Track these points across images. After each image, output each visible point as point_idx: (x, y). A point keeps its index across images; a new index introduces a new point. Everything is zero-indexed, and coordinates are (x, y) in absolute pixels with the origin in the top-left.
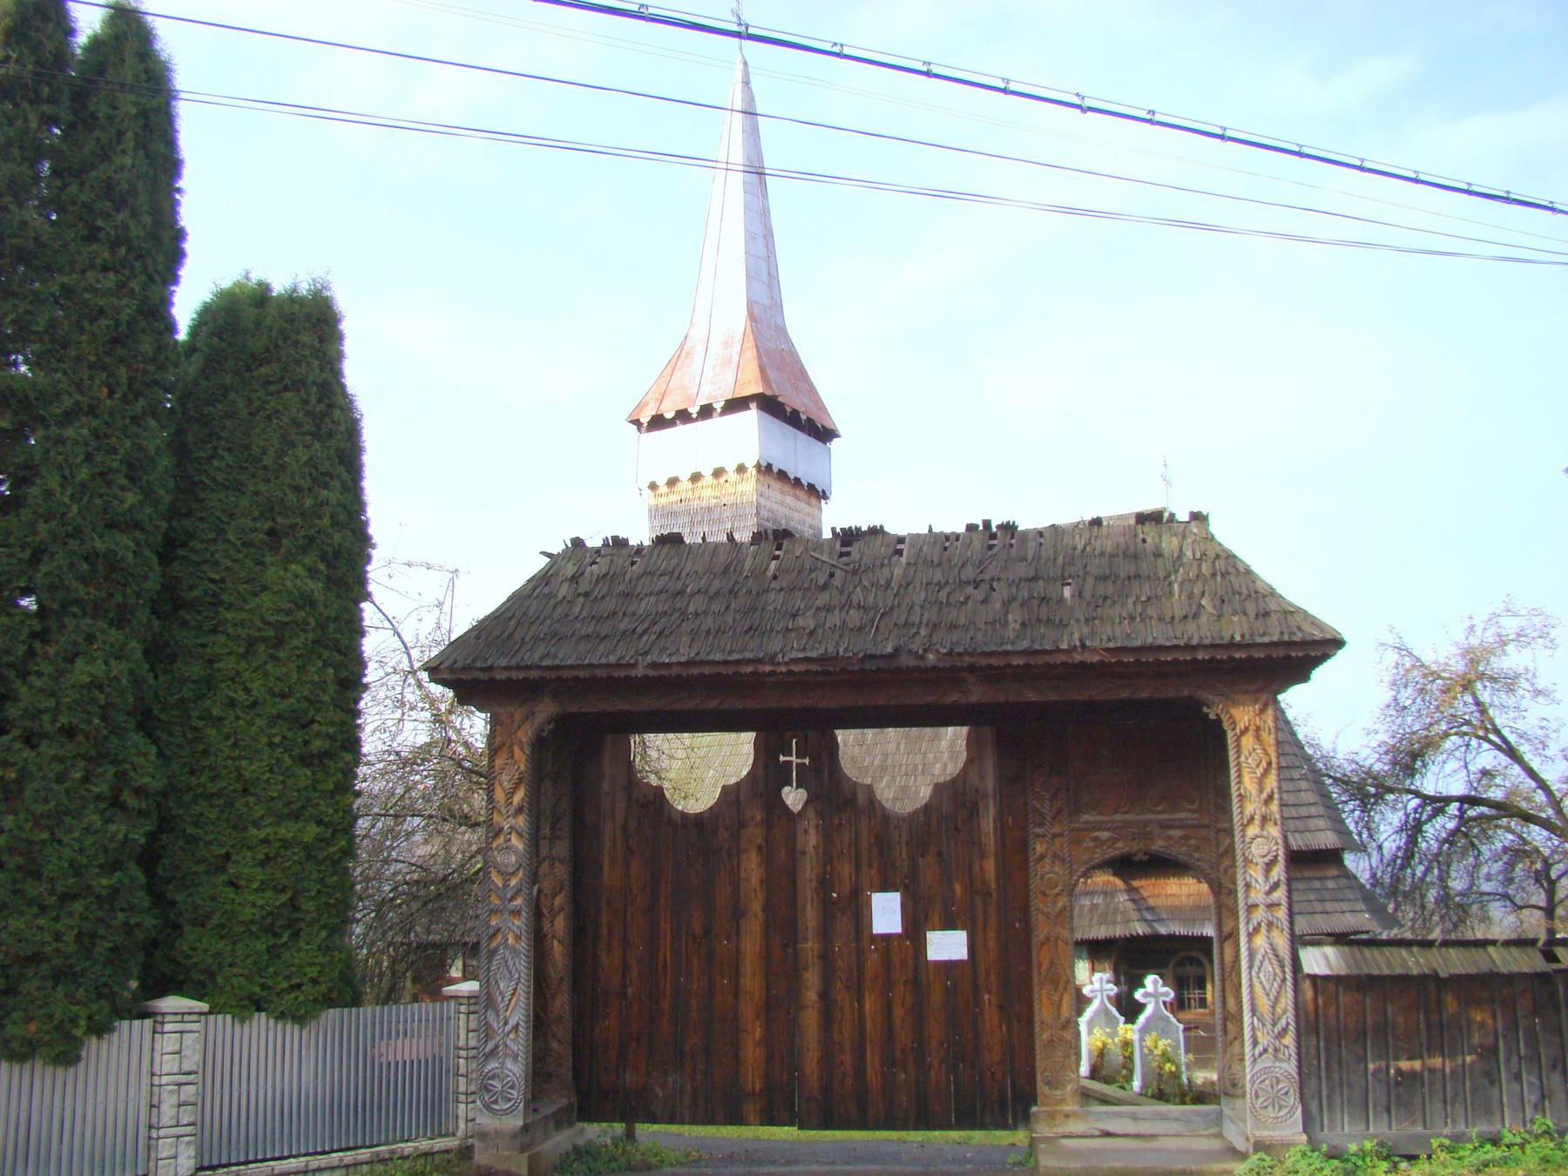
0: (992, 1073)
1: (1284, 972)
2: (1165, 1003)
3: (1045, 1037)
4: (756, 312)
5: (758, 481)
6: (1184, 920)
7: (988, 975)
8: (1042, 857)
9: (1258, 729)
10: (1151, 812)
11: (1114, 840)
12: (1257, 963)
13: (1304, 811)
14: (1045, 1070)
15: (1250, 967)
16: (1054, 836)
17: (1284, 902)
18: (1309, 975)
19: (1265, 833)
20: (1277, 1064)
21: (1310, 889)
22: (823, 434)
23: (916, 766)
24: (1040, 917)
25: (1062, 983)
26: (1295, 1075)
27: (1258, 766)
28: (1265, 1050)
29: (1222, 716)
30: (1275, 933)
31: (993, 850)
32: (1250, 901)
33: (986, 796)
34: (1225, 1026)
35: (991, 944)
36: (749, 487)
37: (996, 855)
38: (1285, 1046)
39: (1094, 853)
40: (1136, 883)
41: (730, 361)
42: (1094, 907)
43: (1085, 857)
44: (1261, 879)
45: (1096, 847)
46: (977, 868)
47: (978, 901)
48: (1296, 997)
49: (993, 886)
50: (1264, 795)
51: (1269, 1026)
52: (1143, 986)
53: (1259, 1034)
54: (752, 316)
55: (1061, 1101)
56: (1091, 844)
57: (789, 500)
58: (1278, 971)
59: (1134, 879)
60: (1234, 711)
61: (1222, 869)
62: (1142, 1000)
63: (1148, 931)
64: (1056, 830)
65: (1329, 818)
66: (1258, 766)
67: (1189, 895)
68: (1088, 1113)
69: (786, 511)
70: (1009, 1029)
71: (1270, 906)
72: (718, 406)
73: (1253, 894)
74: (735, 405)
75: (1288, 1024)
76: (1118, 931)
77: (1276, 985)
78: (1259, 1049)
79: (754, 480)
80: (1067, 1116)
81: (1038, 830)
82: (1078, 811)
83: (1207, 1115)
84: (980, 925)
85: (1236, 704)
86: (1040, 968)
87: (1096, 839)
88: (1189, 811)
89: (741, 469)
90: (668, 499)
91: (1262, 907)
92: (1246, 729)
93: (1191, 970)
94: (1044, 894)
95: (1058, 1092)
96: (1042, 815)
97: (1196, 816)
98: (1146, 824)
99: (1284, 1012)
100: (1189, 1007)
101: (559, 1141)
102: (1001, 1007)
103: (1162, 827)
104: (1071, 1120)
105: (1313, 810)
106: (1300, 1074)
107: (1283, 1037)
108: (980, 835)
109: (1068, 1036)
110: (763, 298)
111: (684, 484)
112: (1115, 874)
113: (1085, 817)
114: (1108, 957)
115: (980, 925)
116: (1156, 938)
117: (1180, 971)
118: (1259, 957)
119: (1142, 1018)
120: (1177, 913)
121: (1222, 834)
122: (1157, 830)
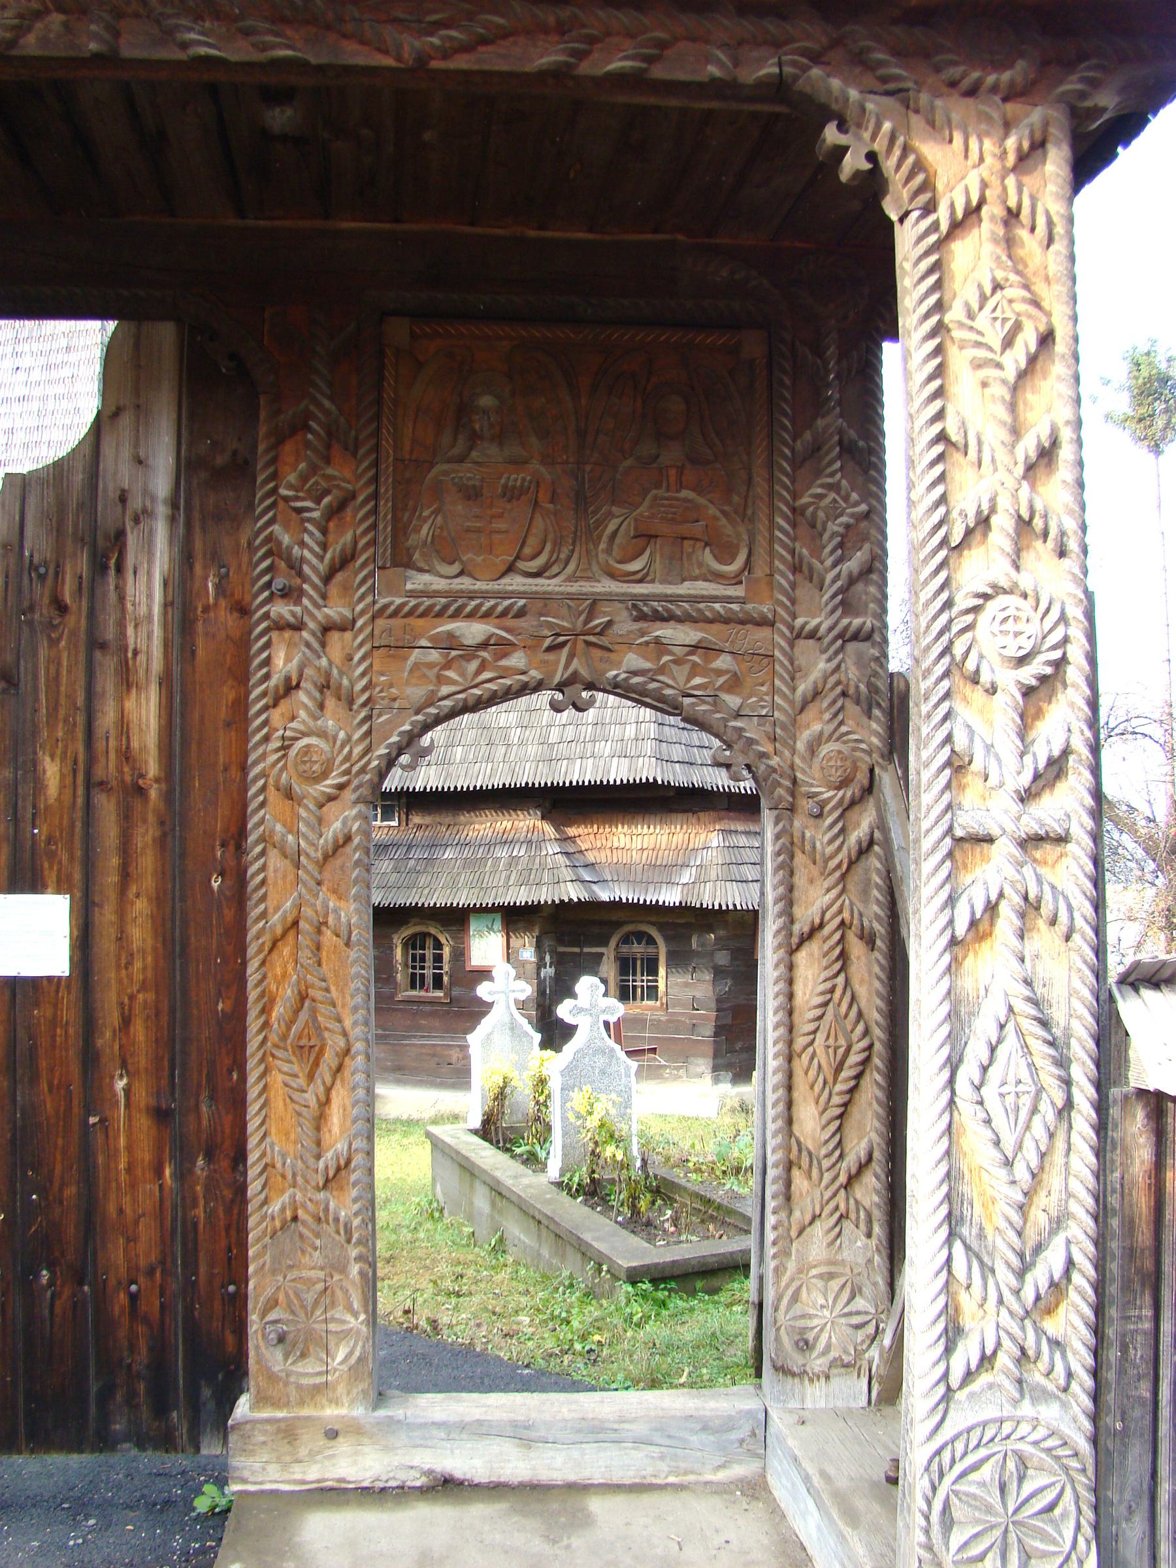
0: (134, 1298)
1: (1067, 1083)
2: (607, 1024)
3: (275, 1207)
6: (632, 883)
7: (126, 1021)
8: (290, 687)
9: (1012, 215)
10: (613, 575)
11: (503, 647)
12: (976, 1052)
14: (272, 1304)
15: (953, 1064)
16: (327, 629)
17: (1080, 827)
18: (1142, 1093)
19: (1025, 581)
20: (1026, 1408)
24: (275, 860)
25: (329, 1059)
26: (1085, 1447)
27: (1008, 343)
28: (987, 1360)
29: (889, 164)
30: (1044, 939)
31: (157, 665)
32: (966, 822)
33: (143, 516)
34: (788, 1183)
35: (140, 935)
37: (166, 680)
38: (1055, 1344)
39: (441, 680)
40: (572, 831)
42: (513, 860)
43: (416, 692)
44: (1008, 744)
45: (447, 665)
46: (107, 718)
47: (107, 808)
48: (1100, 1174)
49: (152, 768)
50: (1028, 446)
51: (1005, 1277)
52: (573, 996)
53: (967, 1303)
55: (318, 1391)
56: (435, 656)
58: (1049, 1076)
59: (570, 826)
60: (930, 151)
61: (800, 746)
62: (569, 1019)
63: (584, 896)
64: (335, 611)
66: (1008, 343)
67: (642, 849)
68: (392, 1424)
70: (183, 1175)
71: (1032, 842)
73: (972, 794)
75: (1070, 1264)
76: (545, 895)
77: (1038, 1129)
78: (967, 1353)
80: (333, 1434)
81: (282, 610)
82: (402, 560)
83: (728, 1424)
84: (110, 879)
85: (938, 128)
86: (265, 1010)
87: (450, 643)
88: (717, 577)
91: (1004, 849)
92: (973, 212)
93: (637, 949)
94: (289, 794)
95: (309, 1367)
96: (295, 567)
97: (738, 591)
98: (595, 604)
99: (1058, 1223)
100: (634, 998)
102: (161, 1115)
103: (642, 617)
104: (343, 1446)
106: (1095, 1441)
107: (1049, 1311)
108: (121, 625)
109: (344, 1206)
113: (418, 581)
114: (528, 928)
115: (110, 879)
116: (594, 906)
117: (625, 949)
118: (983, 1029)
119: (570, 1048)
120: (623, 872)
121: (802, 644)
122: (625, 626)
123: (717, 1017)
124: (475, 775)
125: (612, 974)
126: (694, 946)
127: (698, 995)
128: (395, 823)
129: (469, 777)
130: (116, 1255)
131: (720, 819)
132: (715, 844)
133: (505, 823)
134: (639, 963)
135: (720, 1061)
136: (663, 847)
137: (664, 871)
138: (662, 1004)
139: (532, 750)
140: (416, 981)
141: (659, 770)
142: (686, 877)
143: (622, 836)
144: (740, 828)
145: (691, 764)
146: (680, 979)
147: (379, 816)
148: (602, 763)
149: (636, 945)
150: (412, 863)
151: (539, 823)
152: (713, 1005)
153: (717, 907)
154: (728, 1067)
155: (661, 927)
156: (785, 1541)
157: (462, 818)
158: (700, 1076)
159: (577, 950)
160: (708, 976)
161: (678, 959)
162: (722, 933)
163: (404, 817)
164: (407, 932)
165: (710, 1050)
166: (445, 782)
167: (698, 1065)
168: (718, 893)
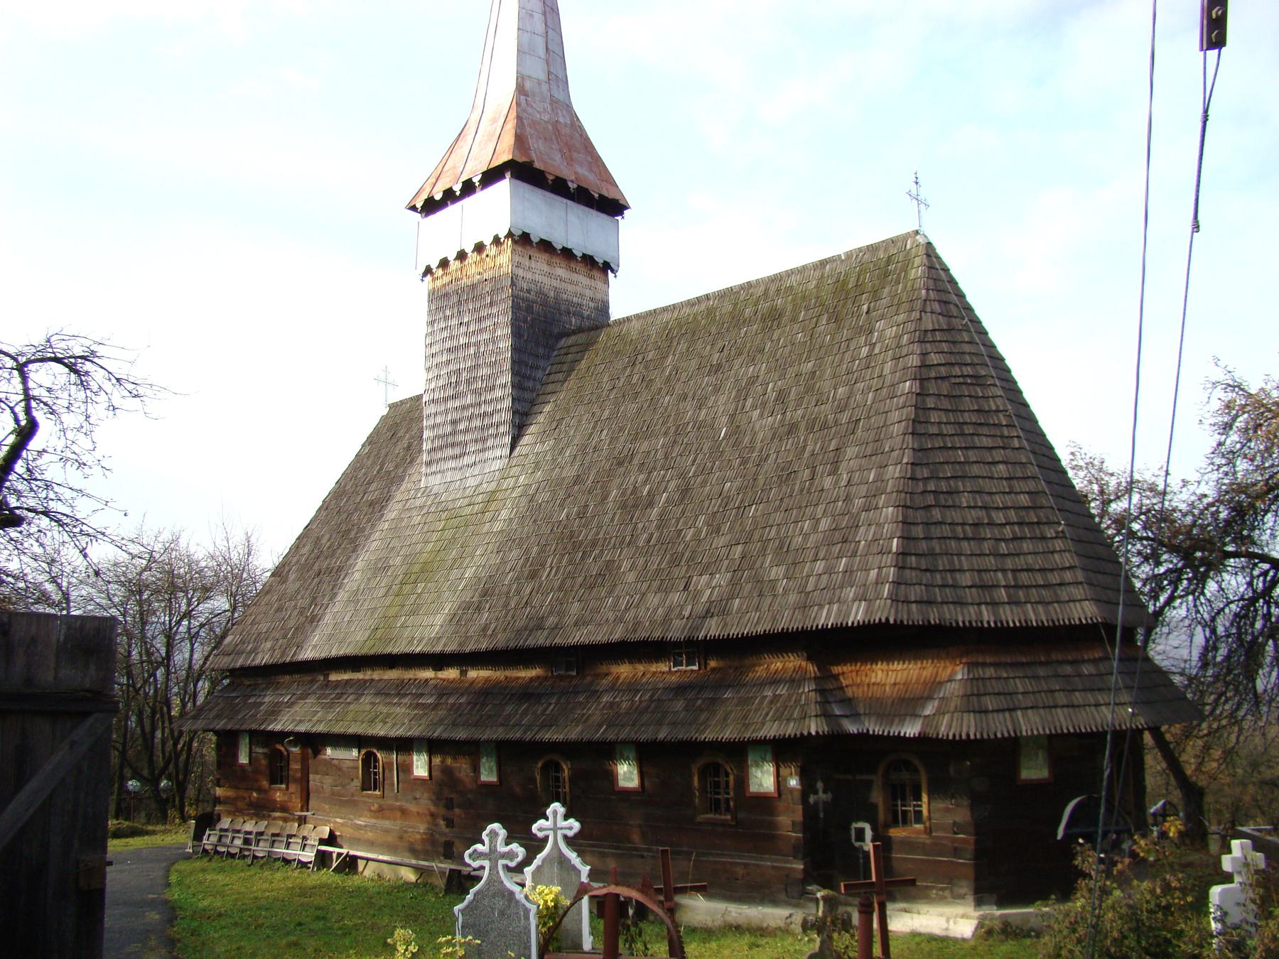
4: (528, 85)
5: (513, 251)
13: (1054, 578)
21: (1057, 676)
22: (613, 207)
23: (624, 537)
36: (504, 259)
41: (494, 134)
42: (776, 698)
54: (521, 90)
57: (561, 272)
59: (838, 664)
65: (1090, 584)
69: (556, 283)
72: (476, 180)
74: (491, 177)
79: (509, 251)
89: (497, 241)
90: (442, 279)
93: (905, 776)
101: (1276, 904)
105: (1068, 576)
110: (537, 70)
111: (454, 265)
112: (809, 659)
123: (976, 842)
124: (745, 622)
128: (695, 668)
129: (740, 625)
130: (247, 740)
132: (959, 677)
133: (778, 664)
136: (913, 682)
137: (907, 704)
138: (926, 828)
139: (793, 598)
140: (716, 806)
141: (893, 611)
142: (929, 710)
143: (880, 673)
144: (988, 660)
146: (940, 804)
147: (684, 661)
148: (845, 607)
150: (699, 702)
151: (804, 664)
153: (951, 737)
156: (388, 846)
157: (746, 661)
158: (962, 897)
159: (849, 777)
161: (939, 789)
163: (703, 662)
164: (701, 762)
166: (721, 631)
167: (962, 887)
168: (954, 724)
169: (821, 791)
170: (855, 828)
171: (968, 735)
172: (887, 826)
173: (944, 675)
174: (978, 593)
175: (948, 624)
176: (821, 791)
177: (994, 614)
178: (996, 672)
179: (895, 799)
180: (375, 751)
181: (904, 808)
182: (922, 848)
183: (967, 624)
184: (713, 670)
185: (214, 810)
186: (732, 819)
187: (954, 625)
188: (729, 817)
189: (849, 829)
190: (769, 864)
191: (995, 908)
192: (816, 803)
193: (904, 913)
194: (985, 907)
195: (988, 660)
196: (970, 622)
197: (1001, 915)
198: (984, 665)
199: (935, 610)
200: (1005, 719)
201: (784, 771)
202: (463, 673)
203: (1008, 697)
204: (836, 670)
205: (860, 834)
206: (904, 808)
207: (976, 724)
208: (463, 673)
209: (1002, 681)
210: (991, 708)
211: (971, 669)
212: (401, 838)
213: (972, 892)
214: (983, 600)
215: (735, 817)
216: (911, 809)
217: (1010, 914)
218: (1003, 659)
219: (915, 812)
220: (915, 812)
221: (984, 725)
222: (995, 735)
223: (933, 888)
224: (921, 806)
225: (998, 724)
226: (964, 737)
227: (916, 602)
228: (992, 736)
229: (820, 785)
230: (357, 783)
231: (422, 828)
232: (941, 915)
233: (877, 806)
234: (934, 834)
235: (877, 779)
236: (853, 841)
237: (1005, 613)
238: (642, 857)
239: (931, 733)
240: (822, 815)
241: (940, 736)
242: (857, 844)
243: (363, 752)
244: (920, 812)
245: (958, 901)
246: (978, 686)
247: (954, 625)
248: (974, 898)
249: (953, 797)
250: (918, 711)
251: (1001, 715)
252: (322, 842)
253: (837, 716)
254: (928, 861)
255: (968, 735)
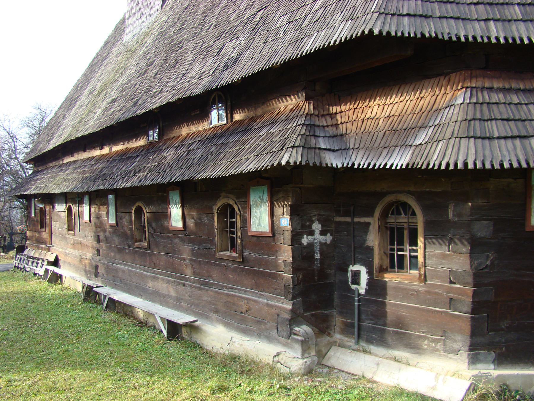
93: (403, 219)
123: (475, 294)
125: (377, 243)
126: (451, 215)
127: (456, 268)
131: (471, 78)
134: (406, 233)
135: (480, 340)
138: (420, 275)
141: (379, 23)
144: (496, 85)
145: (426, 17)
149: (403, 215)
152: (470, 279)
154: (489, 346)
155: (419, 197)
158: (456, 352)
159: (348, 219)
160: (465, 249)
162: (481, 202)
163: (229, 115)
165: (467, 327)
167: (455, 341)
169: (317, 233)
170: (351, 270)
171: (466, 164)
172: (382, 270)
173: (442, 102)
174: (486, 9)
175: (446, 38)
176: (317, 233)
177: (504, 30)
178: (505, 97)
179: (392, 243)
180: (71, 205)
181: (399, 253)
182: (415, 295)
183: (471, 39)
184: (238, 122)
185: (25, 244)
186: (239, 257)
187: (454, 39)
188: (237, 255)
189: (347, 271)
190: (265, 301)
191: (492, 366)
192: (311, 245)
193: (392, 362)
194: (479, 366)
195: (496, 86)
196: (474, 38)
197: (499, 376)
198: (491, 89)
199: (432, 24)
200: (515, 148)
201: (279, 211)
202: (111, 148)
203: (520, 124)
204: (334, 109)
205: (356, 275)
206: (399, 253)
207: (476, 151)
208: (111, 148)
209: (512, 106)
210: (496, 135)
211: (474, 92)
212: (80, 261)
213: (467, 348)
214: (491, 16)
215: (242, 255)
216: (407, 253)
217: (509, 376)
218: (514, 85)
219: (411, 257)
220: (411, 257)
221: (488, 153)
222: (502, 165)
223: (425, 338)
224: (416, 251)
225: (505, 153)
226: (460, 166)
227: (408, 15)
228: (497, 166)
229: (317, 227)
230: (66, 226)
231: (89, 255)
232: (431, 370)
233: (372, 250)
234: (428, 282)
235: (374, 222)
236: (350, 283)
237: (518, 30)
238: (184, 285)
239: (421, 163)
240: (318, 256)
241: (431, 166)
242: (353, 287)
243: (68, 205)
244: (416, 257)
245: (450, 355)
246: (481, 111)
247: (454, 39)
248: (469, 355)
249: (451, 241)
250: (409, 142)
251: (509, 142)
252: (50, 263)
253: (320, 149)
254: (423, 310)
255: (466, 164)
